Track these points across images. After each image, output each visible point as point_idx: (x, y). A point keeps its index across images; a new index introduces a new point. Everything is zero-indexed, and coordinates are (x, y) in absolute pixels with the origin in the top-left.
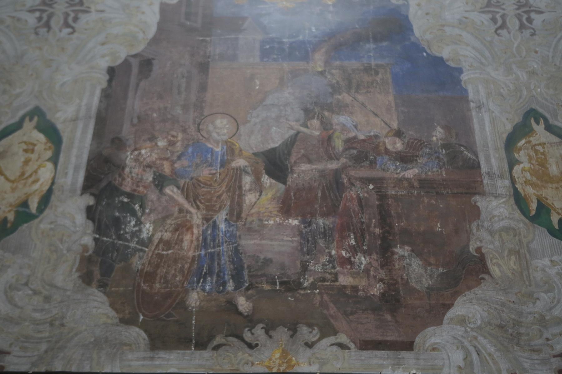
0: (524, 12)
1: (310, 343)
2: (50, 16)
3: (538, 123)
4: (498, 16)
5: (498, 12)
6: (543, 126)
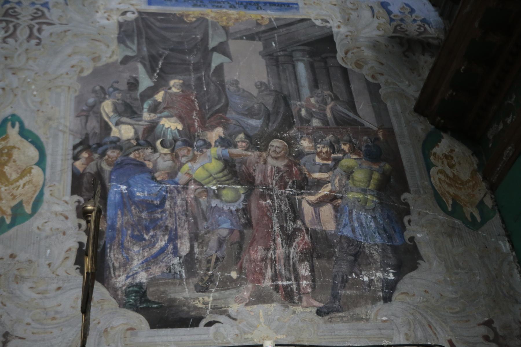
0: (37, 23)
5: (12, 22)
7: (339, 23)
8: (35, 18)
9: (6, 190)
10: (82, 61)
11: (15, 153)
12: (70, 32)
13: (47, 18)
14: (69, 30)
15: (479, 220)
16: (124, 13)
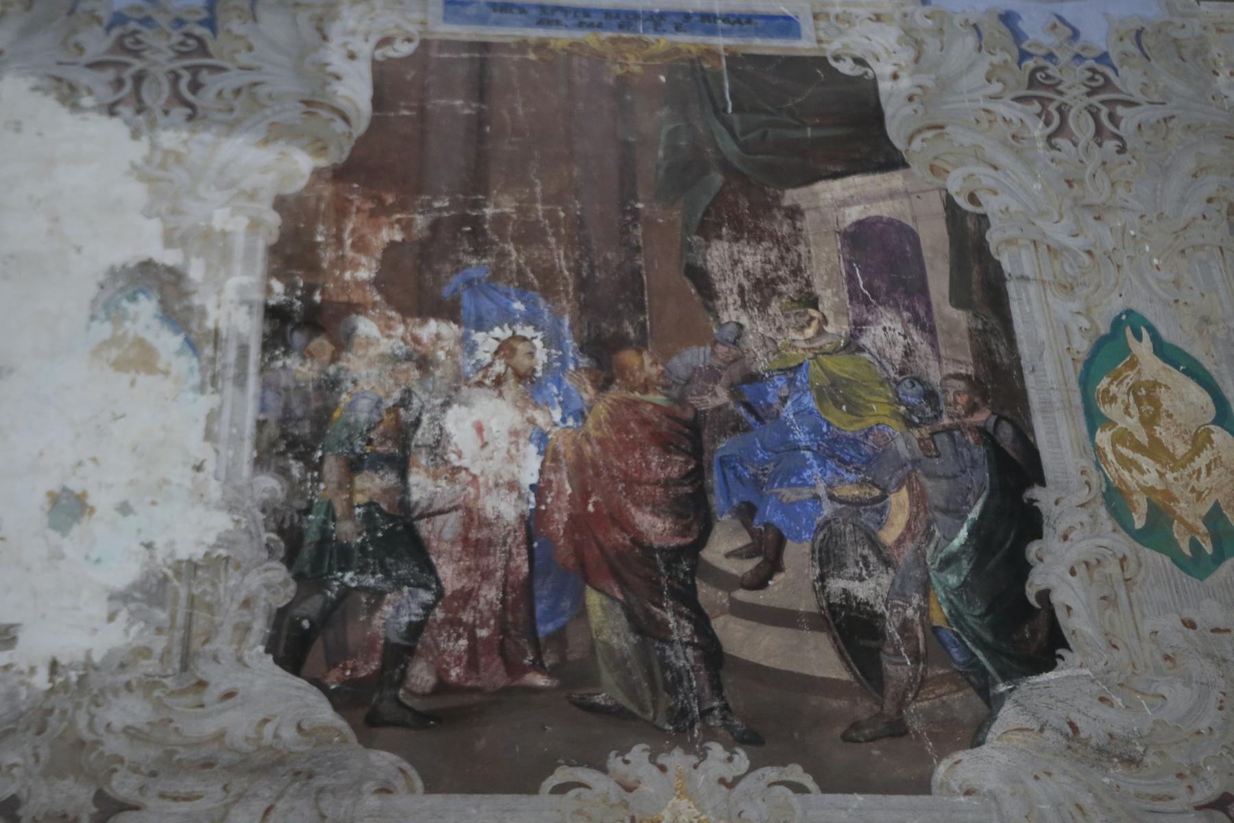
0: (1103, 102)
1: (729, 780)
2: (139, 78)
3: (1139, 337)
4: (1052, 108)
5: (1051, 100)
6: (1150, 345)
7: (895, 68)
8: (1092, 92)
9: (1175, 479)
10: (1224, 188)
11: (1162, 394)
12: (1175, 121)
13: (1118, 91)
14: (1173, 117)
15: (1208, 548)
16: (386, 41)
